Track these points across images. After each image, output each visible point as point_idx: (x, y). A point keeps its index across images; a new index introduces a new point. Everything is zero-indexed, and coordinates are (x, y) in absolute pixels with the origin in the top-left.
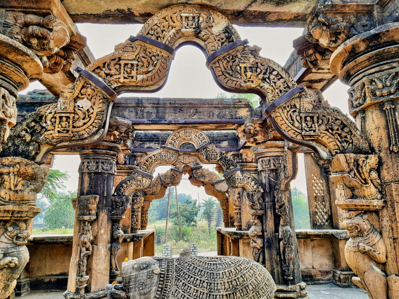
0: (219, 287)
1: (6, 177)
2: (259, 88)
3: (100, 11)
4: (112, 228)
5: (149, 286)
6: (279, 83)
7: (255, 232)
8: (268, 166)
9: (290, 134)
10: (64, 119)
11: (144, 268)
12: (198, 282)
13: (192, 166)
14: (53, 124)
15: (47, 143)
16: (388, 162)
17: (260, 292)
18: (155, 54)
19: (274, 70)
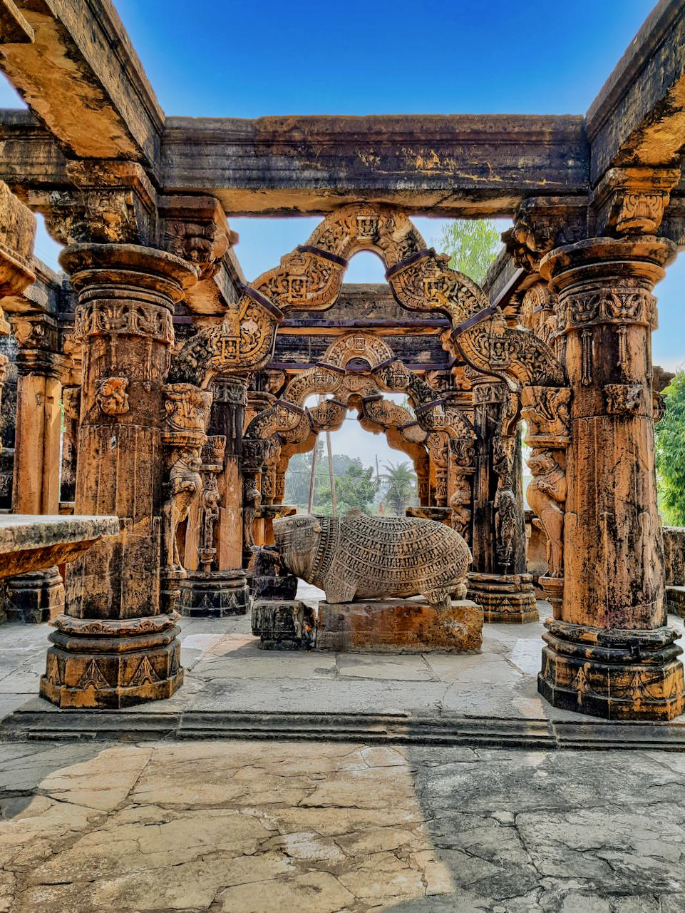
0: (396, 549)
2: (444, 308)
3: (262, 209)
6: (469, 302)
7: (460, 500)
8: (487, 398)
9: (476, 363)
10: (231, 343)
11: (301, 526)
12: (370, 543)
13: (365, 396)
14: (219, 348)
15: (214, 370)
16: (579, 397)
17: (448, 558)
18: (327, 268)
19: (463, 286)
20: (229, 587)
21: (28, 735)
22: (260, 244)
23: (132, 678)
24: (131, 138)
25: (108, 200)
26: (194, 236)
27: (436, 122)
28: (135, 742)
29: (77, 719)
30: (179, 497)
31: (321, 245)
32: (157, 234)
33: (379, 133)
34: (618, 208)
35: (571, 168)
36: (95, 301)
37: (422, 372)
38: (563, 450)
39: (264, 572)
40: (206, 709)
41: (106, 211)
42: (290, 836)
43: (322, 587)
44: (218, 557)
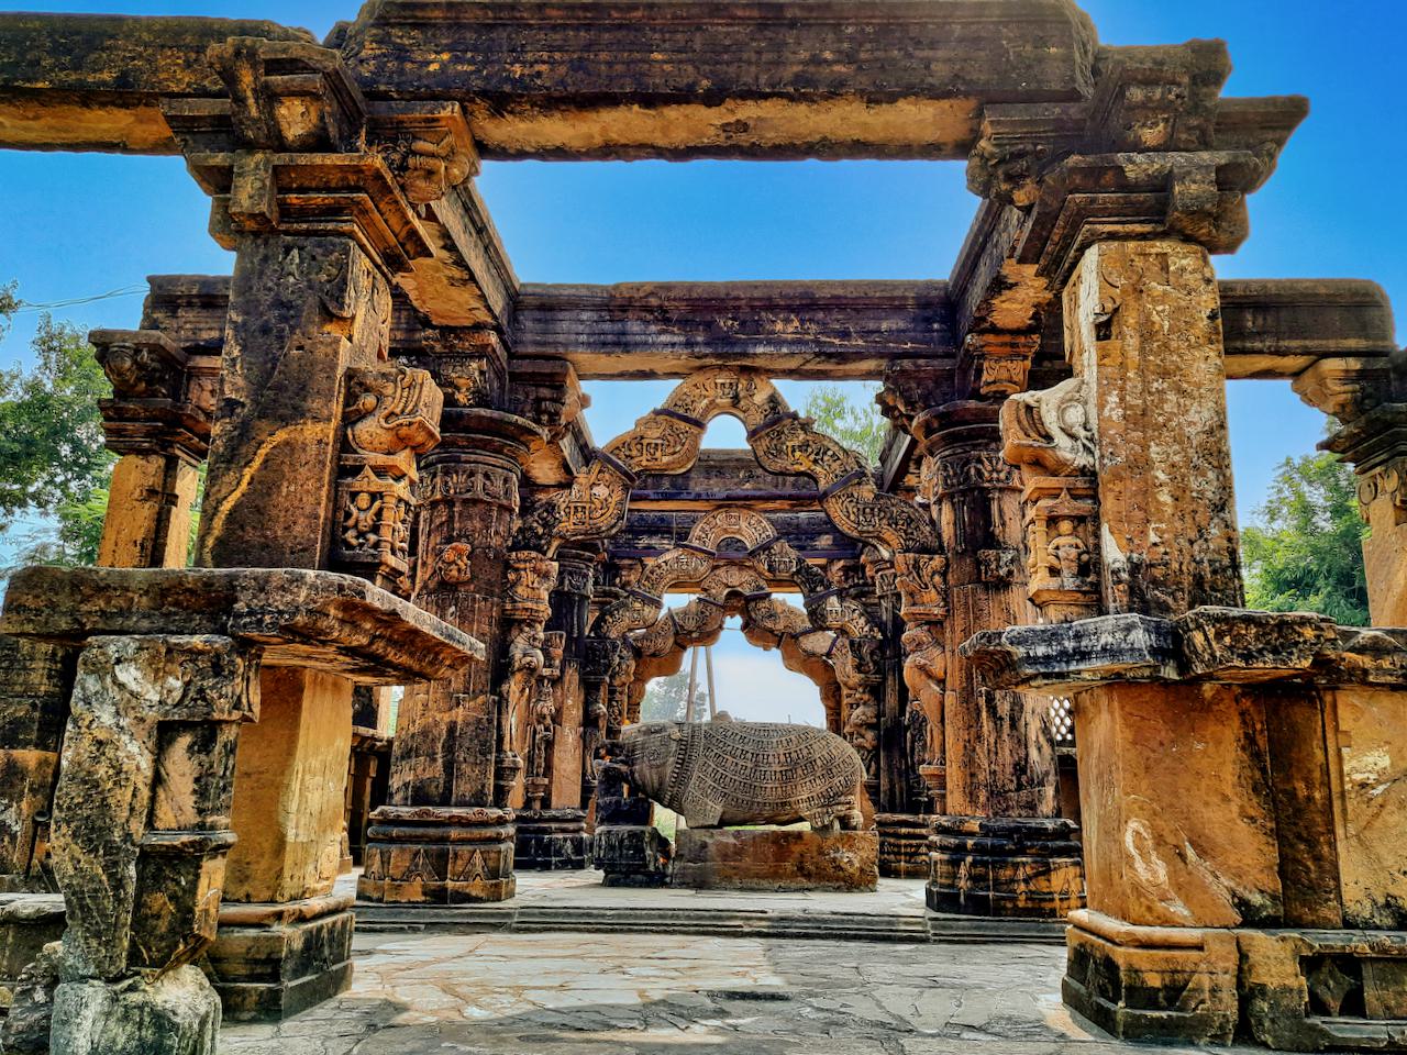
4: (586, 698)
6: (835, 465)
11: (656, 732)
12: (739, 752)
14: (567, 514)
17: (834, 770)
20: (564, 831)
22: (612, 409)
24: (489, 309)
26: (545, 399)
27: (795, 288)
30: (518, 676)
33: (737, 299)
34: (979, 372)
35: (937, 331)
37: (822, 561)
38: (940, 623)
43: (680, 811)
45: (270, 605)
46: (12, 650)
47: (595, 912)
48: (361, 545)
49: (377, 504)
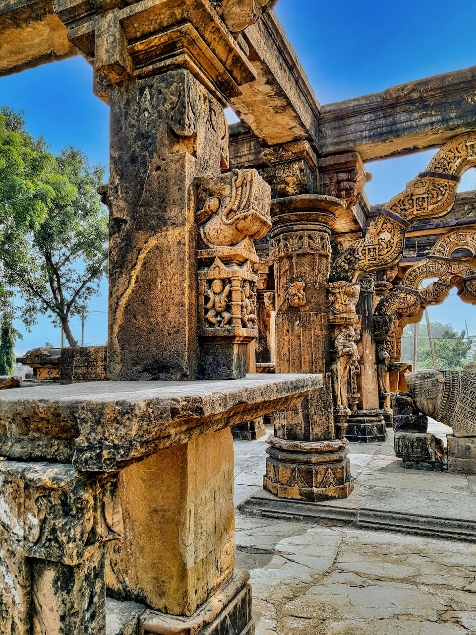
1: (338, 295)
4: (376, 349)
5: (435, 392)
10: (372, 250)
11: (428, 378)
13: (465, 277)
15: (360, 270)
18: (443, 185)
20: (371, 421)
21: (261, 513)
22: (384, 180)
23: (322, 482)
24: (302, 125)
25: (288, 169)
26: (343, 181)
28: (329, 526)
29: (289, 506)
30: (342, 359)
31: (437, 169)
32: (318, 184)
36: (281, 235)
39: (401, 412)
40: (375, 509)
41: (287, 176)
42: (462, 612)
43: (449, 424)
44: (362, 400)
45: (106, 439)
46: (88, 356)
47: (411, 517)
48: (219, 322)
49: (227, 288)
